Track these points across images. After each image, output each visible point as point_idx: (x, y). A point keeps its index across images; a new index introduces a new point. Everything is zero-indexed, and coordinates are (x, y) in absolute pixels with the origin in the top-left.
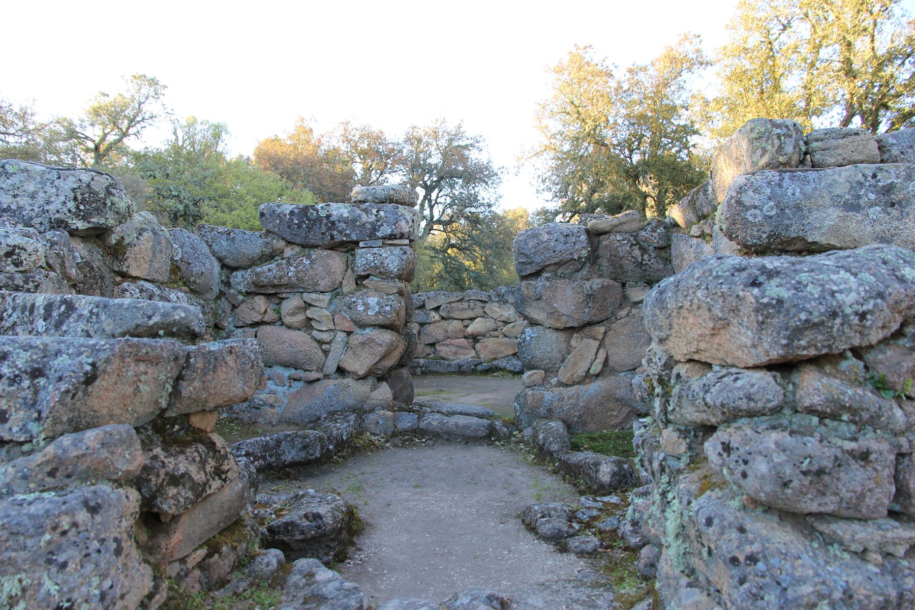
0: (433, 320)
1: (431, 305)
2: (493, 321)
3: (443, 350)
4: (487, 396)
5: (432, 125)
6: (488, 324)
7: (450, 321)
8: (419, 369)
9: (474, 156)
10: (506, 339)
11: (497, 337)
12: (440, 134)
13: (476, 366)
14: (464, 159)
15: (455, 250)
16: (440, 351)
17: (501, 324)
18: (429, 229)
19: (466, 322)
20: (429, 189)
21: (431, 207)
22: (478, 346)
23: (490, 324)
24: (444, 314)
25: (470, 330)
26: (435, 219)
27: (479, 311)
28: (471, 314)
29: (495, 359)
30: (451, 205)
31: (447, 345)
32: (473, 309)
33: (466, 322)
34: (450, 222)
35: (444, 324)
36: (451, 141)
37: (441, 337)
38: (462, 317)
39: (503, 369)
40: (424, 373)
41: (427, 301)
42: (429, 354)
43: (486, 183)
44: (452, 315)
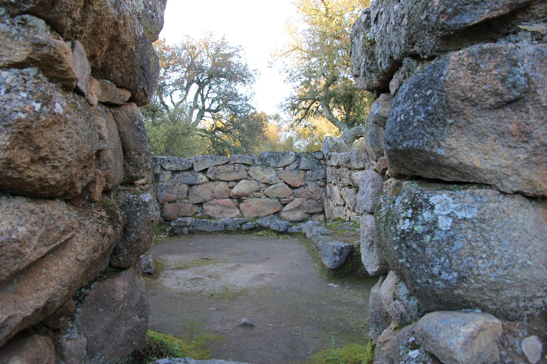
0: (201, 181)
1: (199, 167)
2: (256, 183)
3: (210, 209)
4: (260, 268)
5: (203, 38)
6: (252, 185)
7: (217, 182)
8: (186, 229)
9: (234, 60)
10: (267, 199)
11: (260, 197)
12: (210, 44)
13: (241, 225)
14: (228, 65)
15: (220, 133)
16: (207, 210)
17: (263, 185)
18: (201, 116)
19: (231, 184)
20: (201, 85)
21: (203, 101)
22: (242, 205)
23: (254, 186)
24: (211, 176)
25: (235, 191)
26: (206, 108)
27: (243, 174)
28: (236, 176)
29: (257, 217)
30: (217, 99)
31: (214, 205)
32: (238, 172)
33: (231, 184)
34: (217, 110)
35: (211, 185)
36: (218, 49)
37: (208, 197)
38: (227, 179)
39: (267, 228)
40: (190, 232)
41: (195, 164)
42: (197, 213)
43: (244, 82)
44: (219, 177)
